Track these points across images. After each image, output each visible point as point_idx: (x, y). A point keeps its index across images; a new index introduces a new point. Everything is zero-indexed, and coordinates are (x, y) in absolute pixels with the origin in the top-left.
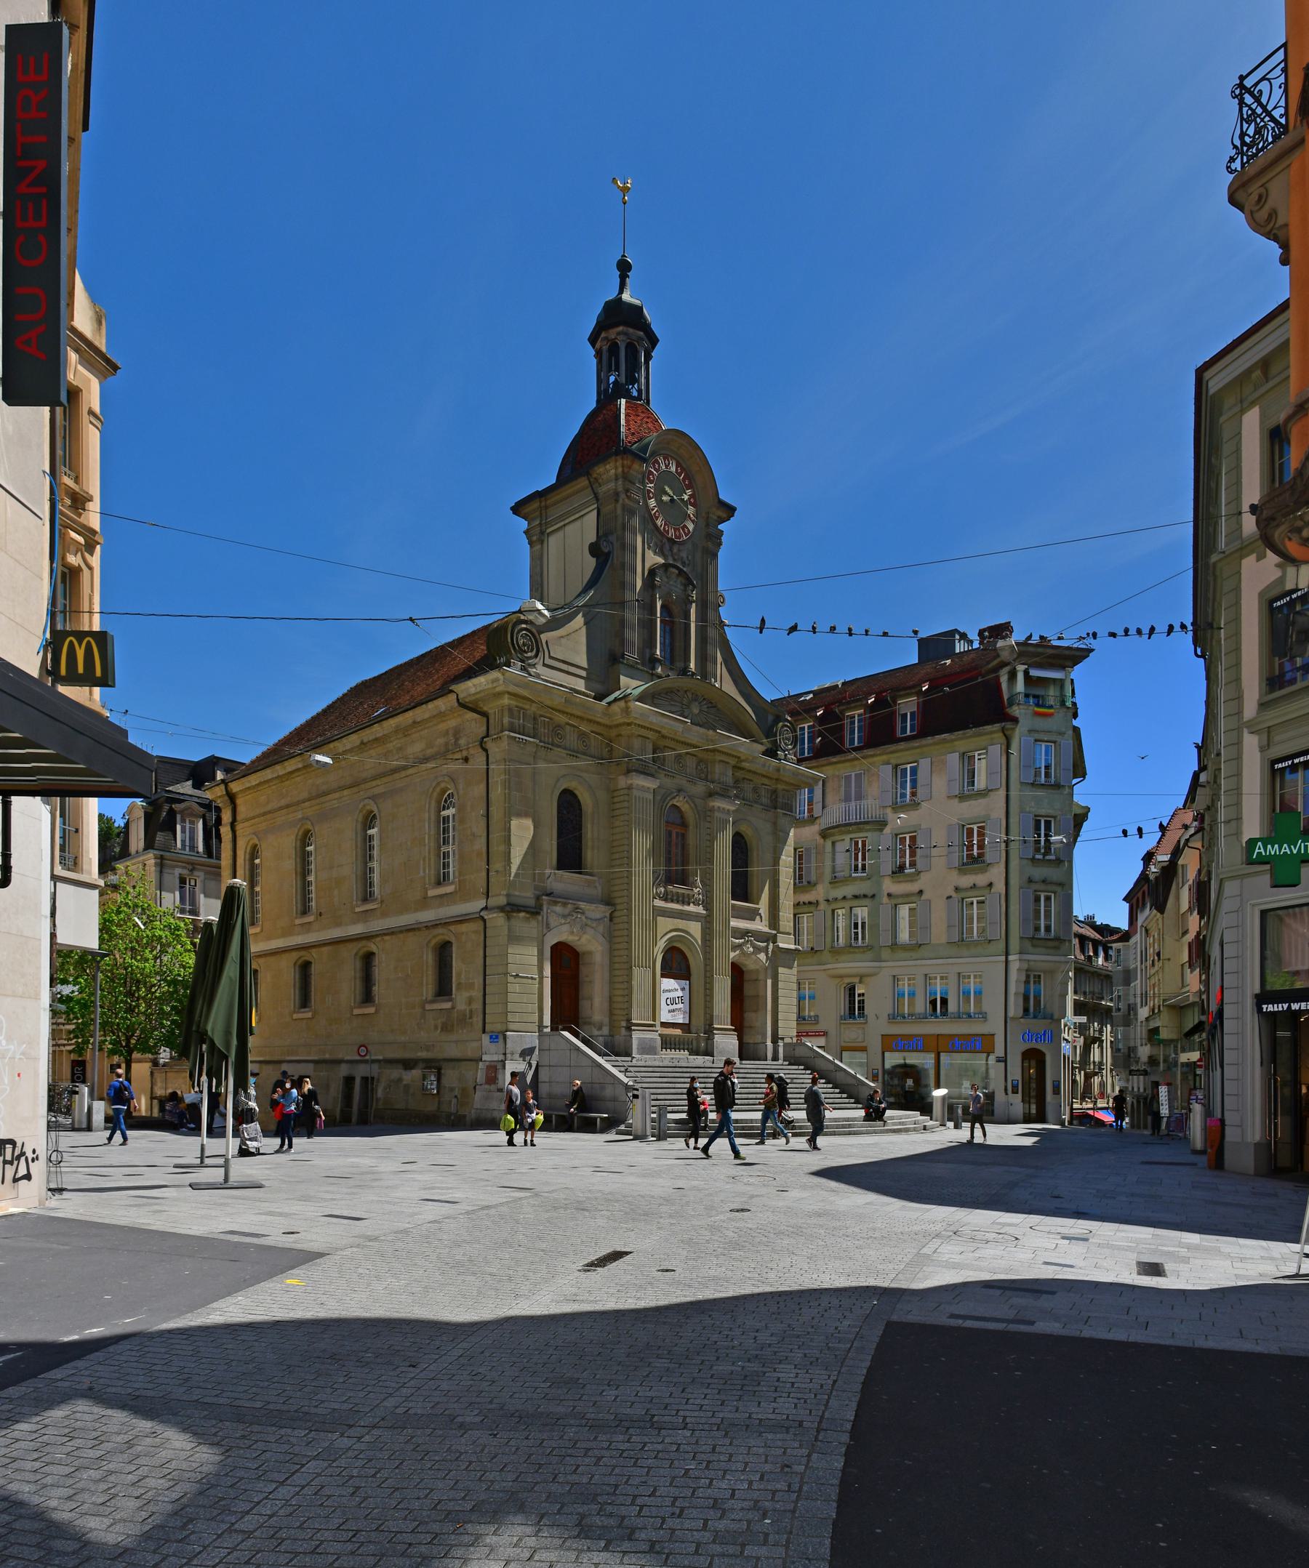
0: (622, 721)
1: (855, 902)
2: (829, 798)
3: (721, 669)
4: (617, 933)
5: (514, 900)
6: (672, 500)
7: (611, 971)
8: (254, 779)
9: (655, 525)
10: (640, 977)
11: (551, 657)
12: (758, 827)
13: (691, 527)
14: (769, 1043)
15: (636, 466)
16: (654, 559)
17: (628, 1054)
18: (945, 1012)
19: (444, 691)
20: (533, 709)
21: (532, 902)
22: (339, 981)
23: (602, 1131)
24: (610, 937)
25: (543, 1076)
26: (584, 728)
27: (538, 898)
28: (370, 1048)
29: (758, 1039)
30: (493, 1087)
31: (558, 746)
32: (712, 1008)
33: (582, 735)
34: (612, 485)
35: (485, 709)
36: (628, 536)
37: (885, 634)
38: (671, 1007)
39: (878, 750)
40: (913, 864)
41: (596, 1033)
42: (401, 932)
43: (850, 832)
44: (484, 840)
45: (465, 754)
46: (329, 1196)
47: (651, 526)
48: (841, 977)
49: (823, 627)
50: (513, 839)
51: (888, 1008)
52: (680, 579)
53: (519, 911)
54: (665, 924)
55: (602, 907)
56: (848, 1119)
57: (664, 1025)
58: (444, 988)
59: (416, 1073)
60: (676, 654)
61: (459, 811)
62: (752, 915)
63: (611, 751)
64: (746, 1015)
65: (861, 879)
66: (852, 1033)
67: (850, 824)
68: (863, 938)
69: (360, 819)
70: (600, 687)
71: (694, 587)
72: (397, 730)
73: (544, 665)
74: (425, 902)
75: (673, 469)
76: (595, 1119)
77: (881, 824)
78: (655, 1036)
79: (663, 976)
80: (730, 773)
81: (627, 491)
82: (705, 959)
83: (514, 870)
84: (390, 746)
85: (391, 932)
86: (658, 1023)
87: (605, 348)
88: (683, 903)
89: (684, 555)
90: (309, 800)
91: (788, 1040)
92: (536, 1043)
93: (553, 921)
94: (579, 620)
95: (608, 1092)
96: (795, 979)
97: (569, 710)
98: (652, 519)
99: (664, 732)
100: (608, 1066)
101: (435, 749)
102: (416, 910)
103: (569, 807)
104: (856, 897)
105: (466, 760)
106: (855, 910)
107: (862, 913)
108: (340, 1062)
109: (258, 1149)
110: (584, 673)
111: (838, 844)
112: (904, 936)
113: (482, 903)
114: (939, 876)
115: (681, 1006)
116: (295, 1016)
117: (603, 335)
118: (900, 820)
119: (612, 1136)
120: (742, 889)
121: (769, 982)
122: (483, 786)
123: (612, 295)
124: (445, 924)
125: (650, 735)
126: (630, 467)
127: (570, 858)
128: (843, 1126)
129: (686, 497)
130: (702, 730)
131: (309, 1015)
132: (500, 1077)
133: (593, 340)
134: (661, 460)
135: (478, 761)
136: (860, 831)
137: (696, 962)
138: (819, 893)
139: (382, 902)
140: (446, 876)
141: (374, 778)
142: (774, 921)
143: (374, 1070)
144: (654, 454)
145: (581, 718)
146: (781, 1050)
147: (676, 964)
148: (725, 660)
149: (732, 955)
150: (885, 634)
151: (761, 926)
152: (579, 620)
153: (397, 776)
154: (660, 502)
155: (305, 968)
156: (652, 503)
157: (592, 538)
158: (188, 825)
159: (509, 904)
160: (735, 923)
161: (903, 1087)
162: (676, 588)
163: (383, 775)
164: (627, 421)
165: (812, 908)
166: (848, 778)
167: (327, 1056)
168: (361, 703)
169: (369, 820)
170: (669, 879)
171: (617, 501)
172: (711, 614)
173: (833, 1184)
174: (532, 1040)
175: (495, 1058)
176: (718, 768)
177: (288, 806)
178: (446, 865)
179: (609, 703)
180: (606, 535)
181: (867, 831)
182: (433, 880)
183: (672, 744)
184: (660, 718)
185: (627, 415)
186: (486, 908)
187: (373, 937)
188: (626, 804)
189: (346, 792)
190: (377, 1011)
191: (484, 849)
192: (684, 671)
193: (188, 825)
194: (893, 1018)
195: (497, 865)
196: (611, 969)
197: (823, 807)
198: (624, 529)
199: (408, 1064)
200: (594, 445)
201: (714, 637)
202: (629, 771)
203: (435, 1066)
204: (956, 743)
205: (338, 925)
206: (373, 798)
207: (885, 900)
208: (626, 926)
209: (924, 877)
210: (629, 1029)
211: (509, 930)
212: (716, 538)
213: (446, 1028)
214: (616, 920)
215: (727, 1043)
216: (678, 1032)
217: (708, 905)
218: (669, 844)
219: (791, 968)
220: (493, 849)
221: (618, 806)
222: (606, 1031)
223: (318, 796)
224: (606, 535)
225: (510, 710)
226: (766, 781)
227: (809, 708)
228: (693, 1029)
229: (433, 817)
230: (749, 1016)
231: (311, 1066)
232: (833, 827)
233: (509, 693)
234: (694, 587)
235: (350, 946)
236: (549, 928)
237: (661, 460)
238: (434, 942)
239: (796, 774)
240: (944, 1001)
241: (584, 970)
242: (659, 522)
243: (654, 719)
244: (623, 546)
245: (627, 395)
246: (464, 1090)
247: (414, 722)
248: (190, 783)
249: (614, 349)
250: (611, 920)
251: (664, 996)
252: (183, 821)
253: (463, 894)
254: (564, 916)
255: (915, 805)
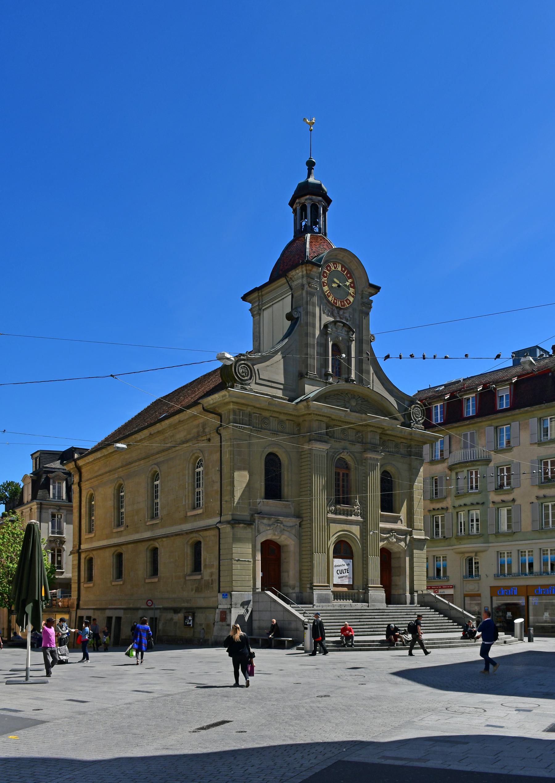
0: (306, 412)
1: (472, 508)
2: (454, 448)
3: (372, 376)
4: (303, 534)
5: (236, 517)
6: (339, 286)
7: (300, 555)
8: (90, 458)
9: (329, 302)
10: (319, 559)
11: (260, 379)
12: (398, 467)
13: (351, 299)
14: (408, 594)
15: (315, 269)
16: (327, 319)
17: (311, 602)
18: (531, 572)
19: (195, 403)
20: (249, 409)
21: (248, 518)
22: (138, 564)
23: (289, 648)
24: (299, 536)
25: (255, 617)
26: (282, 417)
27: (252, 515)
28: (154, 602)
29: (401, 592)
30: (224, 623)
31: (265, 429)
32: (367, 575)
33: (281, 422)
34: (300, 281)
35: (220, 411)
36: (310, 308)
37: (446, 357)
38: (340, 575)
39: (484, 419)
40: (509, 484)
41: (291, 591)
42: (172, 536)
43: (467, 467)
44: (219, 484)
45: (208, 437)
46: (81, 688)
47: (325, 301)
48: (463, 553)
49: (418, 355)
50: (236, 483)
51: (494, 570)
52: (345, 329)
53: (239, 523)
54: (335, 528)
55: (294, 520)
56: (441, 639)
57: (335, 585)
58: (197, 567)
59: (181, 616)
60: (340, 370)
61: (205, 469)
62: (395, 520)
63: (299, 430)
64: (394, 578)
65: (475, 493)
66: (471, 587)
67: (467, 462)
68: (477, 529)
69: (150, 476)
70: (293, 394)
71: (354, 332)
72: (170, 426)
73: (256, 383)
74: (186, 519)
75: (340, 269)
76: (284, 641)
77: (487, 461)
78: (329, 592)
79: (334, 557)
80: (378, 438)
81: (309, 283)
82: (362, 546)
83: (236, 500)
84: (167, 435)
85: (167, 536)
86: (331, 585)
87: (298, 208)
88: (347, 515)
89: (347, 315)
90: (122, 467)
91: (420, 592)
92: (251, 598)
93: (262, 528)
94: (279, 356)
95: (293, 625)
96: (425, 556)
97: (272, 409)
98: (326, 297)
99: (333, 417)
100: (293, 611)
101: (192, 435)
102: (181, 524)
103: (272, 464)
104: (472, 504)
105: (209, 440)
106: (471, 512)
107: (475, 513)
108: (137, 609)
109: (67, 661)
110: (282, 387)
111: (459, 474)
112: (504, 527)
113: (218, 519)
114: (526, 492)
115: (347, 574)
116: (113, 583)
117: (297, 201)
118: (498, 459)
119: (294, 651)
120: (388, 504)
121: (407, 559)
122: (219, 454)
123: (302, 180)
124: (197, 531)
125: (324, 419)
126: (311, 270)
127: (273, 490)
128: (446, 643)
129: (348, 284)
130: (357, 415)
131: (121, 583)
132: (228, 617)
133: (291, 204)
134: (331, 265)
135: (216, 439)
136: (474, 465)
137: (357, 548)
138: (448, 503)
139: (162, 519)
140: (198, 505)
141: (158, 453)
142: (410, 522)
143: (157, 614)
144: (326, 262)
145: (280, 413)
146: (416, 598)
147: (343, 549)
148: (376, 372)
149: (381, 544)
150: (446, 357)
151: (402, 526)
152: (279, 356)
153: (170, 451)
154: (331, 288)
155: (119, 556)
156: (326, 288)
157: (288, 310)
158: (57, 485)
159: (233, 520)
160: (382, 525)
161: (505, 617)
162: (342, 334)
163: (163, 451)
164: (310, 245)
165: (444, 512)
166: (465, 436)
167: (131, 606)
168: (156, 412)
169: (155, 476)
170: (338, 502)
171: (303, 289)
172: (365, 347)
173: (405, 681)
174: (249, 596)
175: (226, 607)
176: (369, 436)
177: (110, 471)
178: (198, 499)
179: (297, 403)
180: (296, 308)
181: (479, 465)
182: (190, 507)
183: (339, 423)
184: (329, 410)
185: (311, 242)
186: (220, 522)
187: (156, 539)
188: (309, 459)
189: (142, 462)
190: (159, 581)
191: (219, 489)
192: (348, 380)
193: (57, 485)
194: (497, 576)
195: (226, 498)
196: (300, 554)
197: (450, 453)
198: (307, 304)
199: (176, 610)
200: (290, 261)
201: (367, 358)
202: (310, 440)
203: (191, 612)
204: (535, 412)
205: (137, 532)
206: (157, 464)
207: (491, 505)
208: (309, 529)
209: (516, 491)
210: (311, 588)
211: (233, 534)
212: (369, 305)
213: (198, 590)
214: (303, 527)
215: (378, 595)
216: (345, 589)
217: (364, 515)
218: (337, 480)
219: (422, 550)
220: (224, 488)
221: (304, 460)
222: (297, 590)
223: (127, 465)
224: (296, 308)
225: (234, 411)
226: (404, 441)
227: (439, 396)
228: (355, 587)
229: (191, 473)
230: (395, 579)
231: (122, 611)
232: (456, 464)
233: (233, 402)
234: (354, 332)
235: (143, 544)
236: (259, 532)
237: (331, 265)
238: (191, 541)
239: (423, 435)
240: (531, 565)
241: (283, 555)
242: (330, 299)
243: (326, 411)
244: (307, 313)
245: (312, 231)
246: (208, 625)
247: (179, 421)
248: (59, 461)
249: (304, 208)
250: (300, 526)
251: (335, 569)
252: (54, 482)
253: (207, 514)
254: (269, 525)
255: (509, 448)
